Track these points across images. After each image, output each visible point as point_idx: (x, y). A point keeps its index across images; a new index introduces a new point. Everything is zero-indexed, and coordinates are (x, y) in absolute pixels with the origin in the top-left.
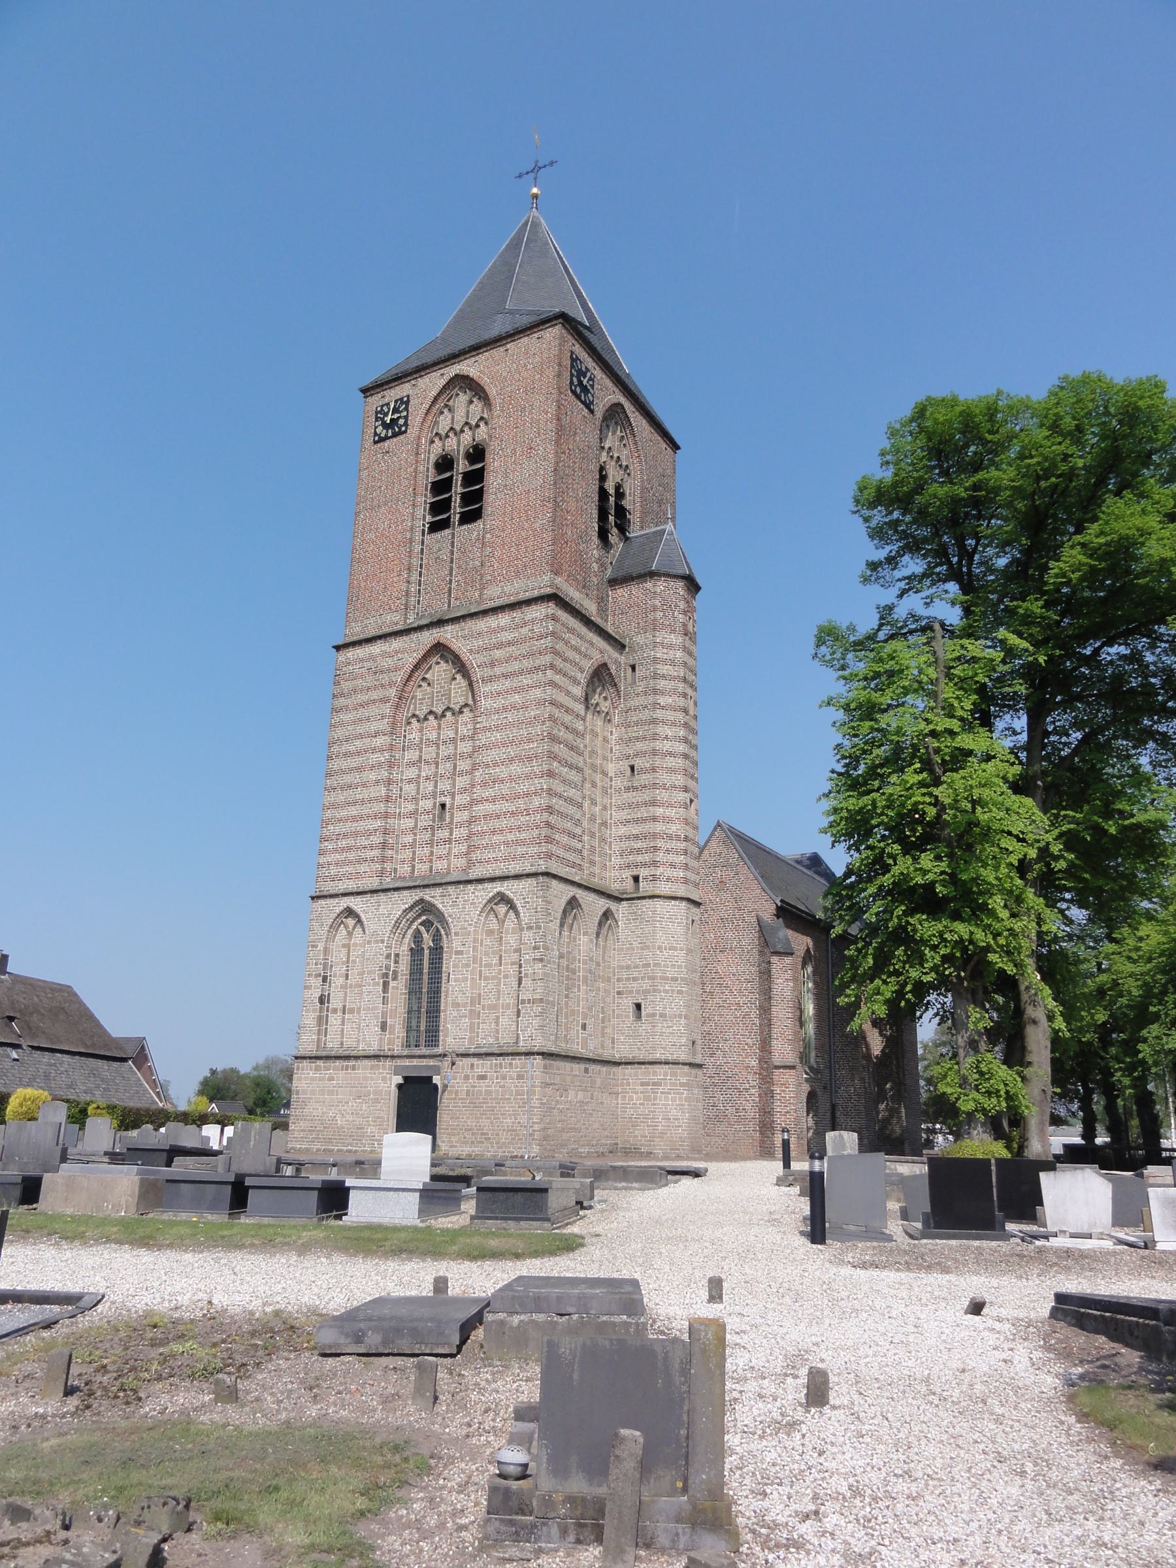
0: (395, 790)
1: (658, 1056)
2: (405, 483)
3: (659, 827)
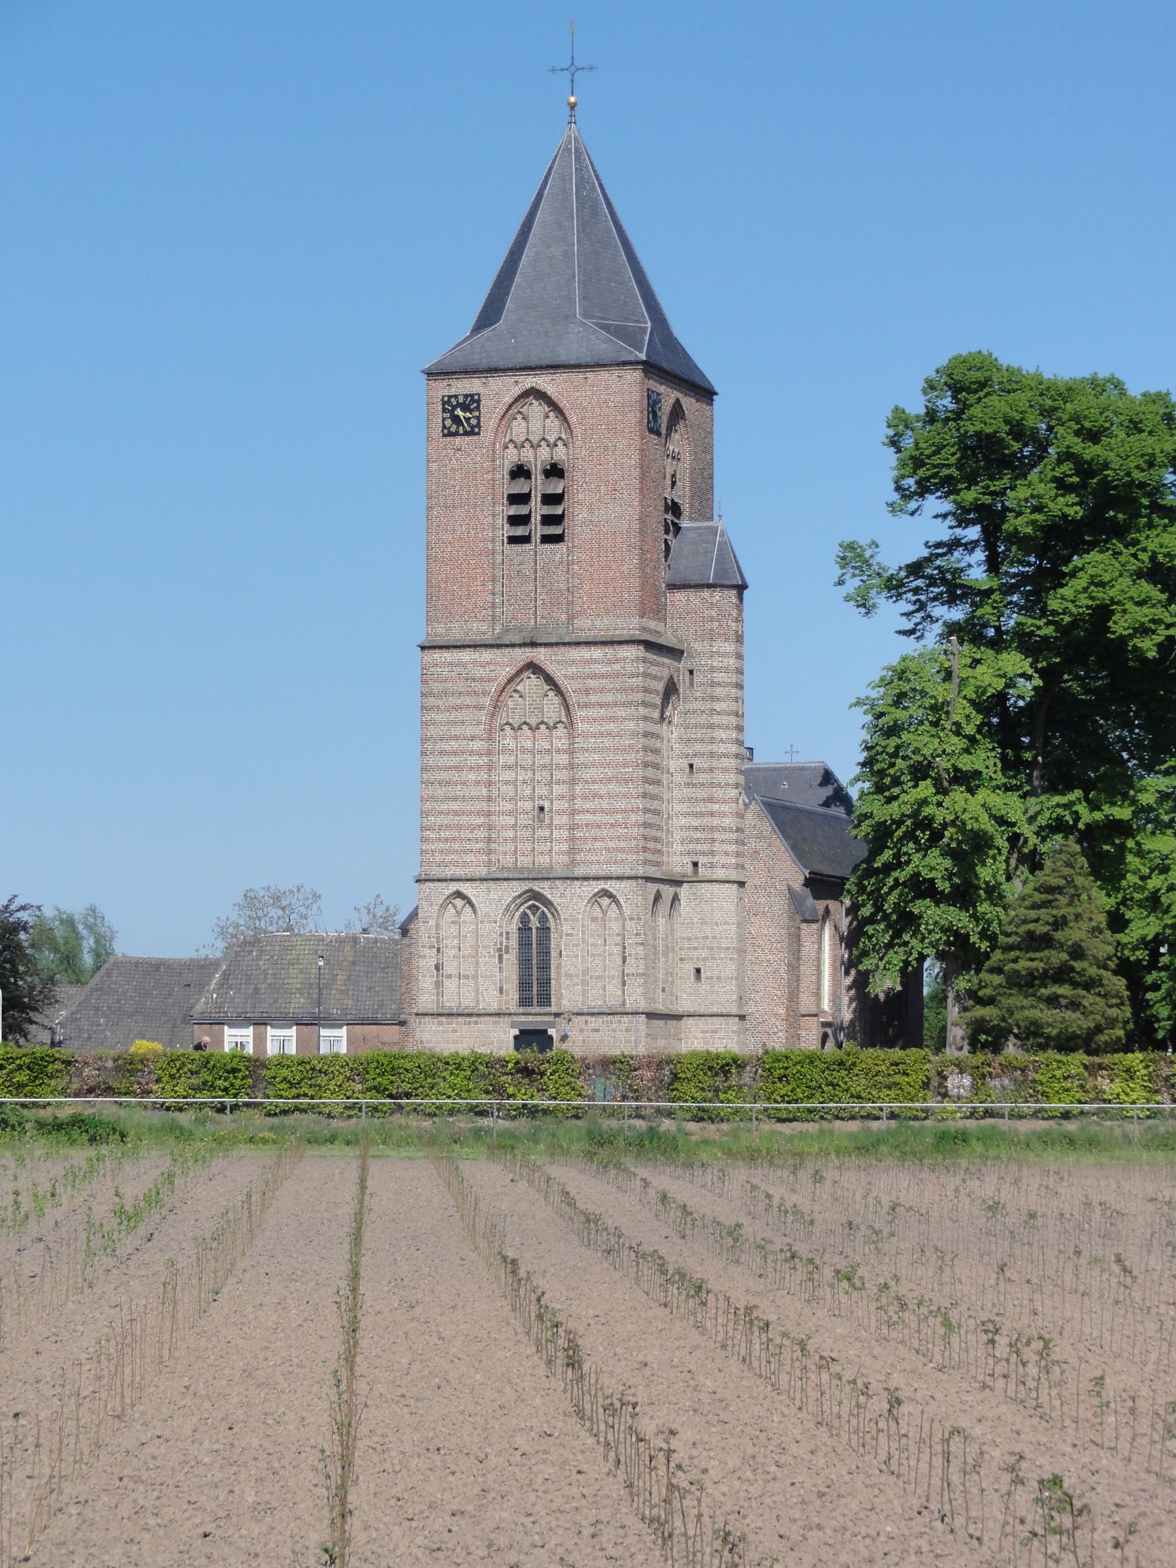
0: (495, 792)
1: (715, 1010)
2: (482, 489)
3: (715, 822)
